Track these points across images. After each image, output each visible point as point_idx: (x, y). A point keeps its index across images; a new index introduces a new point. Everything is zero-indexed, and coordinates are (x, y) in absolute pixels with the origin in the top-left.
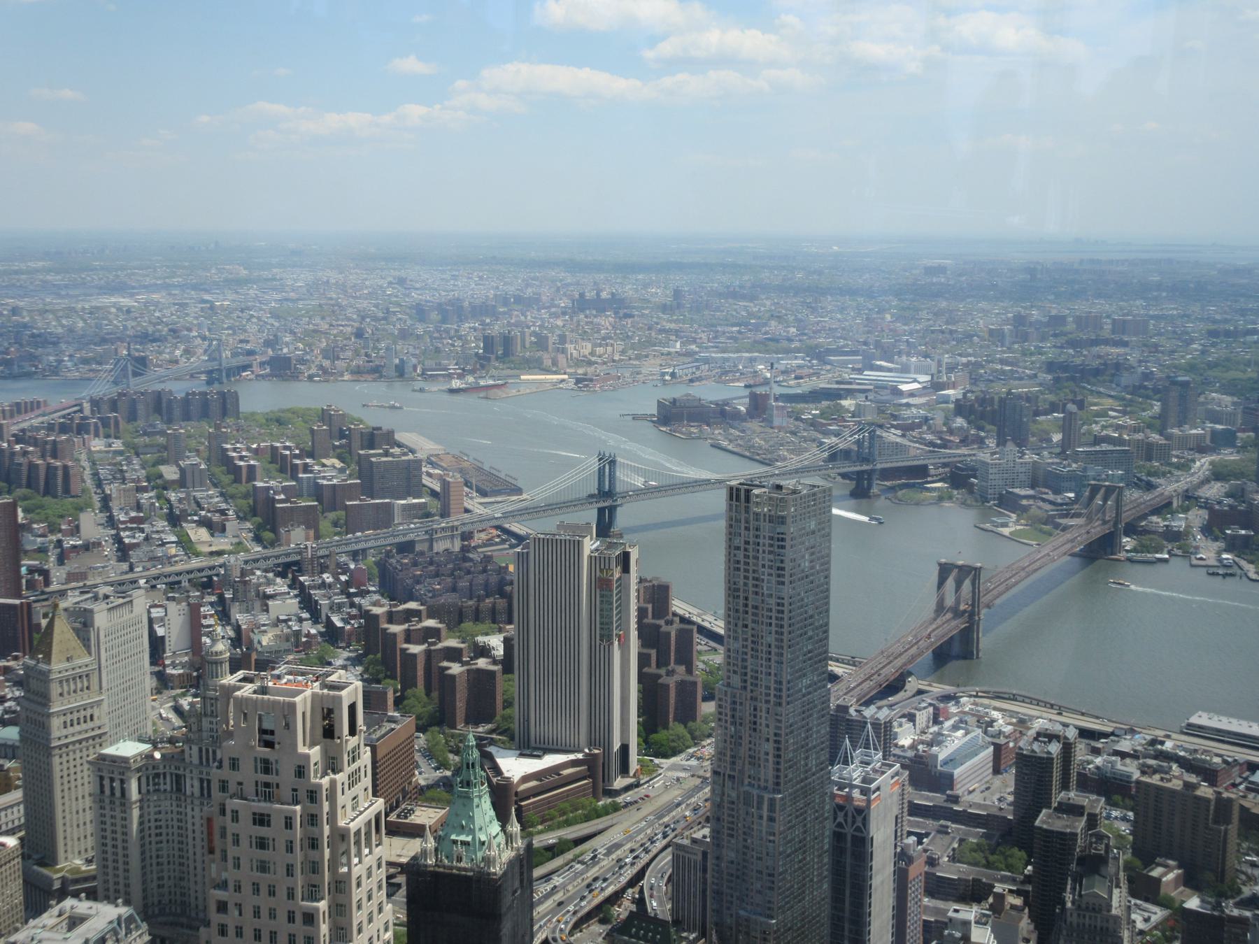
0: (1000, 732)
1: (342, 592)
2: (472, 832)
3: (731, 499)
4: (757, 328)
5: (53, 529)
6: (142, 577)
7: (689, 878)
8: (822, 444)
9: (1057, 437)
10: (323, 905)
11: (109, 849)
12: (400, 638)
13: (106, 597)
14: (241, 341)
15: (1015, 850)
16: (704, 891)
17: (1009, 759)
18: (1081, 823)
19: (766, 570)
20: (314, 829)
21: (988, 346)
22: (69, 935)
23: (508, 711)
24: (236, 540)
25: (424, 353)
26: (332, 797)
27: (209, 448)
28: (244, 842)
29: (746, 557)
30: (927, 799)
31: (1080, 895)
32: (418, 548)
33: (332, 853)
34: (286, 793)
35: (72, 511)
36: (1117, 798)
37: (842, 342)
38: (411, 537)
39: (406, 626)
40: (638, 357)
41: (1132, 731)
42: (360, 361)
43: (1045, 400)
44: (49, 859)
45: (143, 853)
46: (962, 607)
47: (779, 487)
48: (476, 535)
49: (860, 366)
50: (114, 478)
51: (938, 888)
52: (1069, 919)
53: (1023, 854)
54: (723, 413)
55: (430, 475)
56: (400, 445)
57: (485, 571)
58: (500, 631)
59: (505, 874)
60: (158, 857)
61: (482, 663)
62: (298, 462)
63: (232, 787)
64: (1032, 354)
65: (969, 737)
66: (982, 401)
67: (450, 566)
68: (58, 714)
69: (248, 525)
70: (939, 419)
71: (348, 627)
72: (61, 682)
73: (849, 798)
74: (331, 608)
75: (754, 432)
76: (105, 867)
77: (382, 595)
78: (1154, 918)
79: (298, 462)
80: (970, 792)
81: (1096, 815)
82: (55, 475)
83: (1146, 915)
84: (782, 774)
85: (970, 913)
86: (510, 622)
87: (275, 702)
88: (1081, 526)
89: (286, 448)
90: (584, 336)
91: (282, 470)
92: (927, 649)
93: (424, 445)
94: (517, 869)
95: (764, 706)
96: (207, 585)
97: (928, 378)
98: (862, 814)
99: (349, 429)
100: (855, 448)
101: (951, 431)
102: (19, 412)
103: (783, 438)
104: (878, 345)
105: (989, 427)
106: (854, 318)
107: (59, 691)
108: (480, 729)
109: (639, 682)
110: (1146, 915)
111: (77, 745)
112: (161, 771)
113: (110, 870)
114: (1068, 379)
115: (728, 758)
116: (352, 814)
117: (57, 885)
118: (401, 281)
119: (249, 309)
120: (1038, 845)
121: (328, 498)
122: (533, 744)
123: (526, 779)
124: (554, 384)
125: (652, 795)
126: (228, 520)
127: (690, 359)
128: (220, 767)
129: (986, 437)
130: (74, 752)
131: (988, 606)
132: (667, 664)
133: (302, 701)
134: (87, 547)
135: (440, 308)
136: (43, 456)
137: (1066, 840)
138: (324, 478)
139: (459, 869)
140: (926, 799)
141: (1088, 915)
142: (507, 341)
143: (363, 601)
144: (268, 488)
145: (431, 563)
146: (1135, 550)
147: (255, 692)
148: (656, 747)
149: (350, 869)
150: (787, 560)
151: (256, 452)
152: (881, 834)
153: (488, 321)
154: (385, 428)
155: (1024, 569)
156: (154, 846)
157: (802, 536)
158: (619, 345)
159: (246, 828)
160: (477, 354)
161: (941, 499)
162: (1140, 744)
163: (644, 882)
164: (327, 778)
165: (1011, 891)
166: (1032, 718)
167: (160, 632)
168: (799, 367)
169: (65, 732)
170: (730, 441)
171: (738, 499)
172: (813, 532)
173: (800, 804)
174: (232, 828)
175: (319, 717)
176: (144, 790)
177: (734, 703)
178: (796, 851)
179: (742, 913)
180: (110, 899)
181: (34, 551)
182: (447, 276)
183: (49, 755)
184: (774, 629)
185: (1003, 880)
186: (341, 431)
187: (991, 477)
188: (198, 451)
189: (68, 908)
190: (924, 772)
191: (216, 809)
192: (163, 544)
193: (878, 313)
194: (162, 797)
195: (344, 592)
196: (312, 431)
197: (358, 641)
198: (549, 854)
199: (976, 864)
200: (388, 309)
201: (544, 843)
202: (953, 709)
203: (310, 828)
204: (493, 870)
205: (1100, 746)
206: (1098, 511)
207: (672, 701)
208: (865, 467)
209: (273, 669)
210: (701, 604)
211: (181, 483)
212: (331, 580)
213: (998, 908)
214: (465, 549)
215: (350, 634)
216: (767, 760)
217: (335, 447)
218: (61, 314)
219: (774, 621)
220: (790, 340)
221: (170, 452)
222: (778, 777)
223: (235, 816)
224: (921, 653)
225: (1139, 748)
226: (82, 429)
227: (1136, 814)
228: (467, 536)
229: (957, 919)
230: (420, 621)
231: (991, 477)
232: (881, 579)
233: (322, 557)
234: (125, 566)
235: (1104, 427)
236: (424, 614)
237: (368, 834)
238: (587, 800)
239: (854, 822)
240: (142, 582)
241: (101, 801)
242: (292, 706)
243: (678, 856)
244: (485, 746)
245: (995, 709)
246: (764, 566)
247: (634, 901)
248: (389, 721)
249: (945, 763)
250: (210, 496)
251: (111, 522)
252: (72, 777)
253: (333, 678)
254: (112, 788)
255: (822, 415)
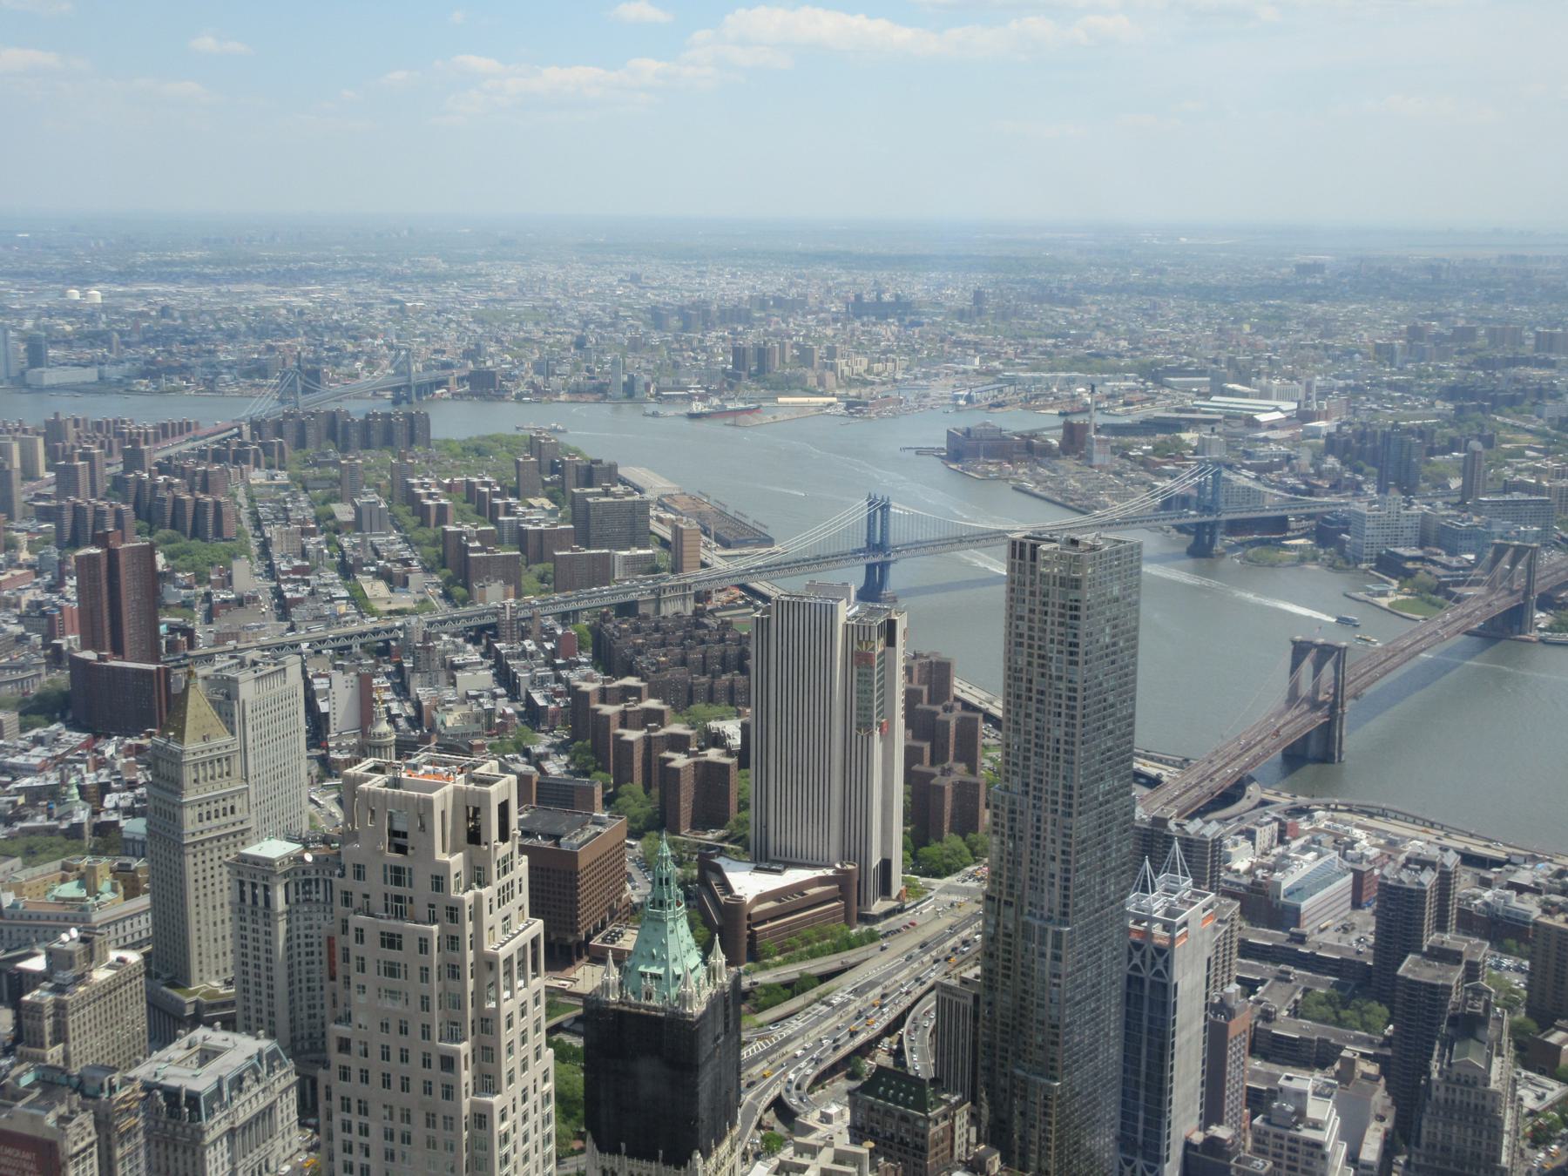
0: (1362, 856)
1: (547, 664)
2: (664, 963)
3: (1013, 556)
4: (1078, 341)
5: (201, 579)
6: (305, 640)
7: (957, 1027)
8: (1153, 487)
9: (1455, 483)
10: (465, 1048)
11: (250, 969)
12: (614, 722)
13: (255, 663)
14: (436, 351)
15: (1374, 1005)
16: (975, 1043)
17: (1370, 892)
18: (1456, 974)
19: (1055, 647)
20: (455, 954)
21: (1373, 366)
22: (199, 1071)
23: (744, 814)
24: (421, 597)
25: (659, 368)
26: (476, 915)
27: (392, 483)
28: (371, 968)
29: (1031, 629)
30: (1265, 937)
31: (1450, 1064)
32: (642, 610)
33: (477, 984)
34: (423, 912)
35: (224, 557)
36: (1511, 942)
37: (1185, 359)
38: (633, 596)
39: (621, 707)
40: (926, 376)
41: (1534, 859)
42: (580, 378)
43: (1443, 436)
44: (180, 979)
45: (290, 975)
46: (1321, 697)
47: (1074, 542)
48: (715, 596)
49: (1208, 390)
50: (276, 518)
51: (1269, 1047)
52: (1434, 1093)
53: (1384, 1010)
54: (1030, 448)
55: (660, 520)
56: (624, 482)
57: (722, 640)
58: (739, 714)
59: (704, 1015)
60: (308, 980)
61: (713, 754)
62: (498, 501)
63: (357, 900)
64: (1429, 376)
65: (1322, 861)
66: (1362, 436)
67: (680, 633)
68: (192, 804)
69: (436, 579)
70: (1305, 458)
71: (553, 706)
72: (196, 766)
73: (1148, 934)
74: (532, 683)
75: (1068, 471)
76: (246, 991)
77: (596, 668)
78: (1550, 1096)
79: (498, 501)
80: (1322, 931)
81: (1477, 964)
82: (205, 513)
83: (1540, 1091)
84: (1070, 902)
85: (1305, 1081)
86: (748, 706)
87: (407, 798)
88: (1480, 597)
89: (485, 484)
90: (860, 349)
91: (479, 512)
92: (1275, 748)
93: (655, 484)
94: (720, 1009)
95: (1050, 817)
96: (383, 652)
97: (1294, 406)
98: (1164, 954)
99: (563, 462)
100: (1194, 493)
101: (1319, 474)
102: (165, 436)
103: (1104, 480)
104: (1231, 362)
105: (1368, 469)
106: (1203, 329)
107: (194, 776)
108: (709, 836)
109: (906, 782)
110: (1540, 1091)
111: (199, 847)
112: (313, 876)
113: (251, 995)
114: (1474, 409)
115: (1004, 880)
116: (501, 937)
117: (190, 1011)
118: (635, 278)
119: (446, 311)
120: (1396, 996)
121: (533, 546)
122: (772, 855)
123: (761, 898)
124: (820, 408)
125: (918, 923)
126: (410, 572)
127: (991, 379)
128: (342, 875)
129: (1364, 482)
130: (212, 851)
131: (1355, 697)
132: (945, 760)
133: (442, 798)
134: (240, 602)
135: (682, 312)
136: (191, 491)
137: (1437, 993)
138: (529, 522)
139: (648, 1008)
140: (1262, 937)
141: (1458, 1088)
142: (762, 354)
143: (571, 675)
144: (460, 534)
145: (657, 629)
146: (1550, 629)
147: (386, 785)
148: (925, 864)
149: (498, 1004)
150: (1081, 633)
151: (449, 488)
152: (1189, 984)
153: (740, 329)
154: (607, 460)
155: (1403, 650)
156: (304, 968)
157: (1100, 604)
158: (903, 361)
159: (372, 951)
160: (724, 370)
161: (1302, 560)
162: (1544, 876)
163: (904, 1030)
164: (471, 893)
165: (1363, 1056)
166: (1405, 839)
167: (324, 707)
168: (1130, 390)
169: (200, 826)
170: (1038, 483)
171: (1022, 556)
172: (1117, 600)
173: (1095, 940)
174: (356, 950)
175: (463, 819)
176: (292, 899)
177: (1012, 812)
178: (1087, 998)
179: (1018, 1072)
180: (250, 1030)
181: (177, 605)
182: (692, 273)
183: (182, 854)
184: (1063, 719)
185: (1358, 1041)
186: (553, 464)
187: (1367, 532)
188: (378, 486)
189: (200, 1040)
190: (1261, 902)
191: (338, 926)
192: (332, 600)
193: (1234, 322)
194: (314, 908)
195: (549, 663)
196: (518, 463)
197: (565, 724)
198: (788, 992)
199: (1324, 1021)
200: (616, 313)
201: (784, 979)
202: (1304, 825)
203: (450, 953)
204: (688, 1011)
205: (1491, 876)
206: (1504, 577)
207: (948, 807)
208: (1206, 518)
209: (410, 757)
210: (979, 687)
211: (357, 525)
212: (533, 648)
213: (1345, 1076)
214: (698, 613)
215: (555, 715)
216: (1053, 884)
217: (545, 484)
218: (219, 315)
219: (1064, 711)
220: (1119, 356)
221: (342, 488)
222: (1066, 905)
223: (360, 936)
224: (1266, 754)
225: (1542, 880)
226: (240, 457)
227: (1532, 964)
228: (703, 597)
229: (1289, 1089)
230: (640, 700)
231: (1367, 532)
232: (1208, 666)
233: (524, 619)
234: (286, 625)
235: (1518, 471)
236: (645, 692)
237: (522, 963)
238: (838, 927)
239: (1153, 965)
240: (304, 646)
241: (242, 911)
242: (429, 804)
243: (943, 1000)
244: (712, 856)
245: (1358, 826)
246: (1052, 641)
247: (891, 1053)
248: (594, 823)
249: (1290, 893)
250: (391, 541)
251: (271, 572)
252: (209, 881)
253: (482, 770)
254: (254, 896)
255: (1156, 450)
